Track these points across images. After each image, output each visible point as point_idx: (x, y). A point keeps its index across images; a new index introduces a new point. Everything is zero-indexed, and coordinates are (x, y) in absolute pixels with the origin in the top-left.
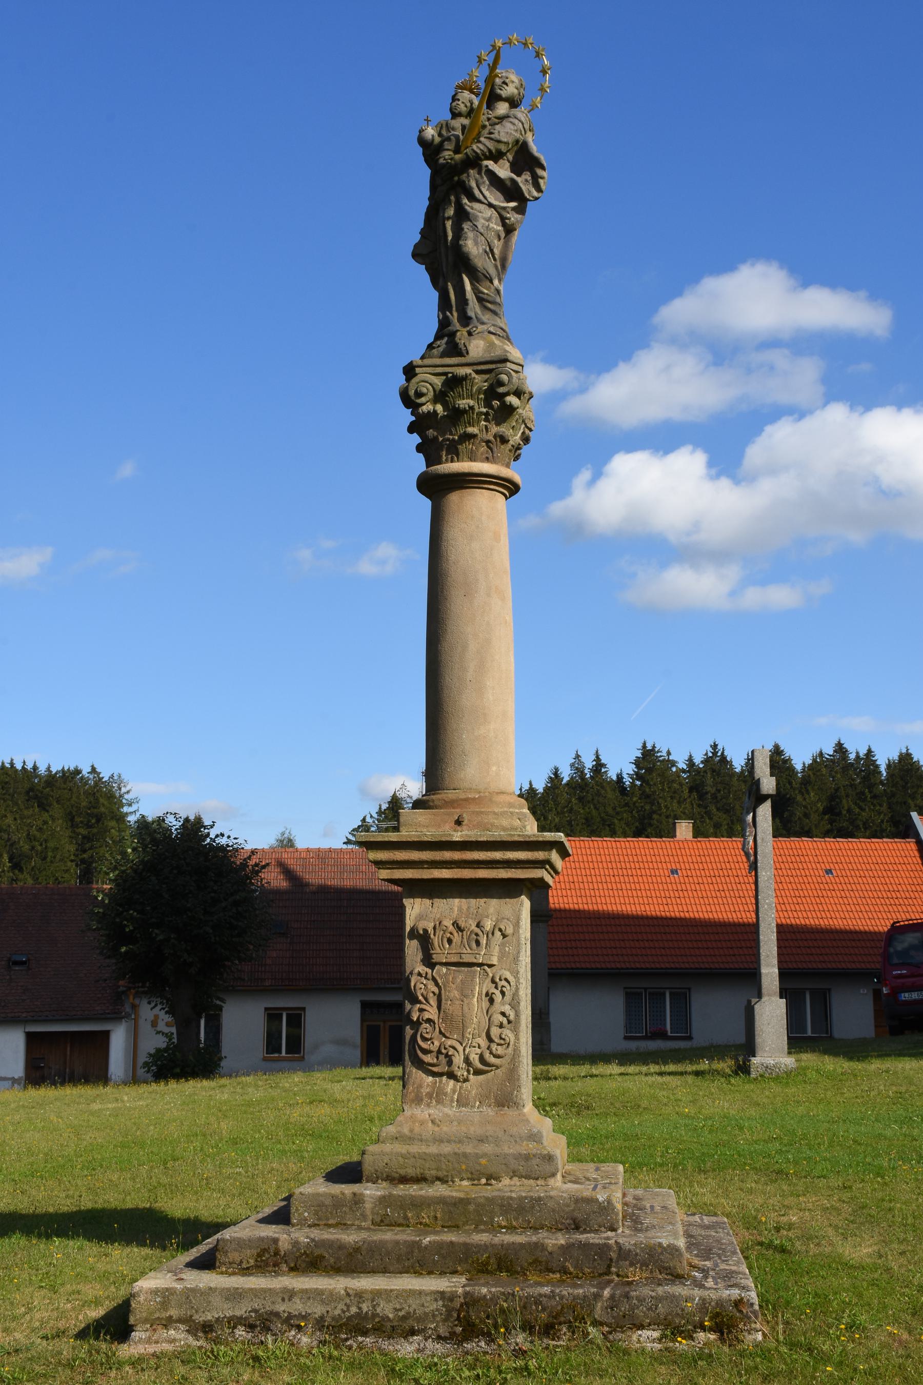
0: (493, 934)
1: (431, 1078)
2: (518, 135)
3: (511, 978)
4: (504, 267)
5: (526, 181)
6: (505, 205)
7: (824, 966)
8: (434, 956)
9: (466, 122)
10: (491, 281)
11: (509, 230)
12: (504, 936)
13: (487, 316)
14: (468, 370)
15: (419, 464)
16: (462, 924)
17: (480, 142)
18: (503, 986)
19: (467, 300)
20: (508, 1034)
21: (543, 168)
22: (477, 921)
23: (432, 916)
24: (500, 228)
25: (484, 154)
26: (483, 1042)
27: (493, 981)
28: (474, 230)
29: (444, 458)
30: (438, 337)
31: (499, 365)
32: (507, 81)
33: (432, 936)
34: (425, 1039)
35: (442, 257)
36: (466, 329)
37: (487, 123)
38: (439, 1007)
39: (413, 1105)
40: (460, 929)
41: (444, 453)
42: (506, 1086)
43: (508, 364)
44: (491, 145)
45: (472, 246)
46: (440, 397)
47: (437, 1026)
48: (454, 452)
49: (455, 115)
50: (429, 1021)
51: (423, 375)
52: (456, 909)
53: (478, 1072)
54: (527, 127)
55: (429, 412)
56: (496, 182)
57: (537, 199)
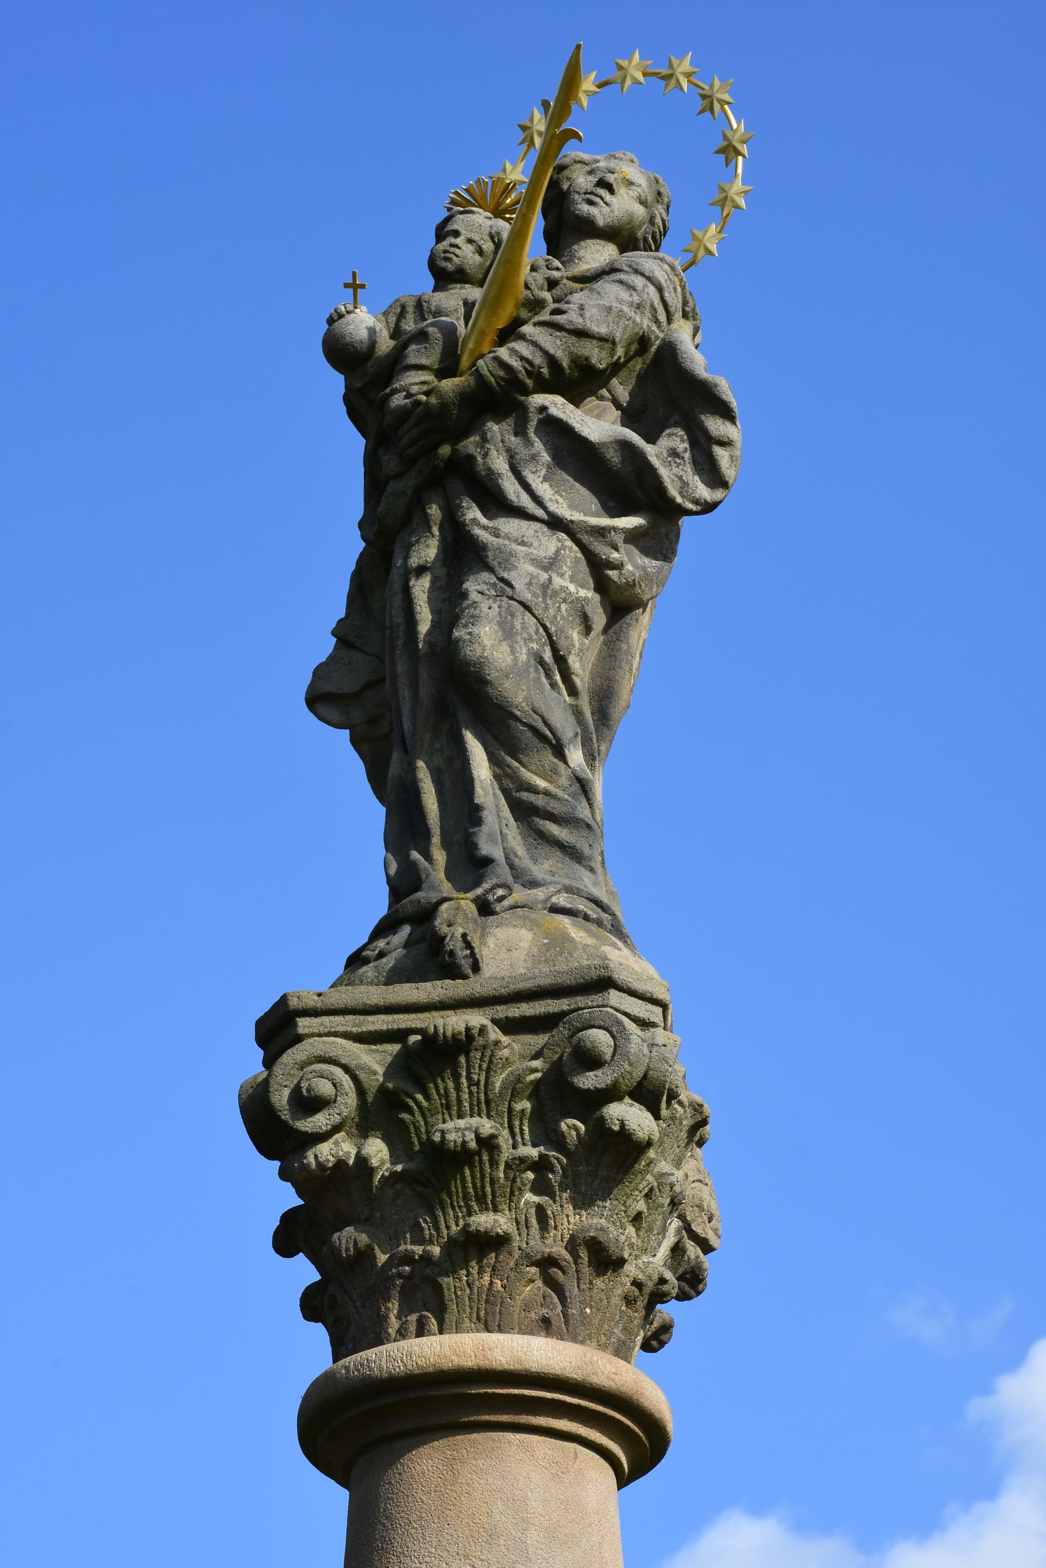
2: (645, 322)
4: (603, 715)
5: (674, 453)
6: (605, 521)
9: (475, 293)
10: (559, 752)
11: (620, 604)
13: (547, 865)
14: (476, 1019)
15: (310, 1353)
17: (522, 337)
19: (477, 809)
21: (727, 413)
24: (588, 593)
25: (533, 372)
28: (501, 594)
29: (394, 1324)
30: (384, 928)
31: (581, 1001)
32: (611, 178)
35: (401, 694)
36: (470, 895)
37: (547, 295)
41: (394, 1307)
43: (614, 997)
44: (555, 344)
45: (495, 643)
46: (380, 1111)
48: (428, 1302)
49: (445, 276)
51: (317, 1038)
54: (675, 300)
55: (340, 1163)
56: (574, 454)
57: (709, 507)
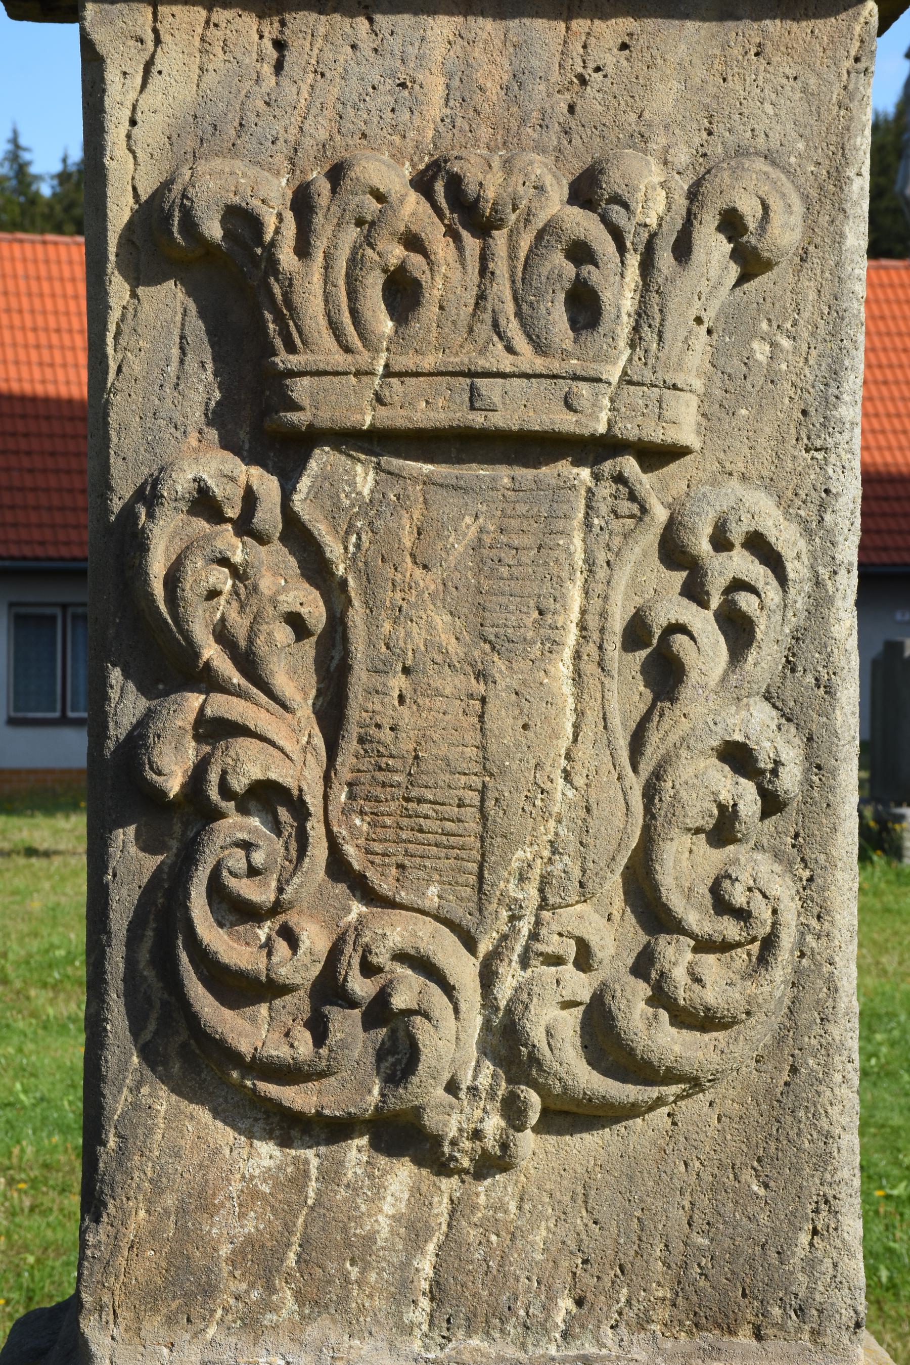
0: (683, 249)
1: (267, 1153)
3: (786, 538)
7: (885, 558)
8: (301, 389)
12: (750, 263)
16: (488, 183)
18: (738, 585)
20: (761, 873)
22: (577, 167)
23: (284, 126)
26: (613, 934)
27: (673, 551)
33: (287, 257)
34: (235, 911)
38: (332, 713)
39: (153, 1325)
40: (471, 215)
42: (742, 1197)
47: (316, 829)
50: (267, 797)
52: (437, 92)
53: (569, 1115)
